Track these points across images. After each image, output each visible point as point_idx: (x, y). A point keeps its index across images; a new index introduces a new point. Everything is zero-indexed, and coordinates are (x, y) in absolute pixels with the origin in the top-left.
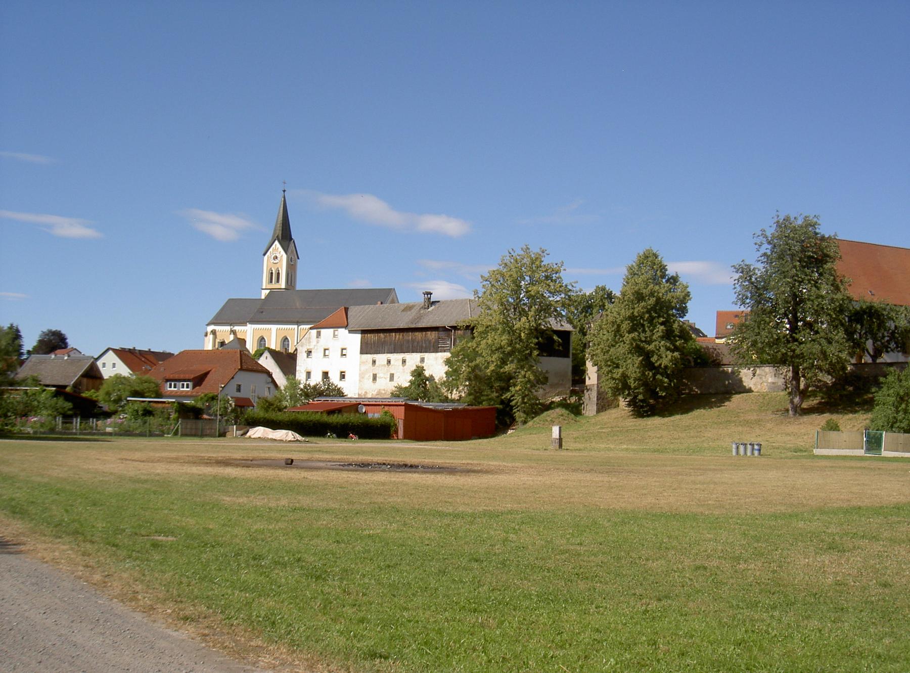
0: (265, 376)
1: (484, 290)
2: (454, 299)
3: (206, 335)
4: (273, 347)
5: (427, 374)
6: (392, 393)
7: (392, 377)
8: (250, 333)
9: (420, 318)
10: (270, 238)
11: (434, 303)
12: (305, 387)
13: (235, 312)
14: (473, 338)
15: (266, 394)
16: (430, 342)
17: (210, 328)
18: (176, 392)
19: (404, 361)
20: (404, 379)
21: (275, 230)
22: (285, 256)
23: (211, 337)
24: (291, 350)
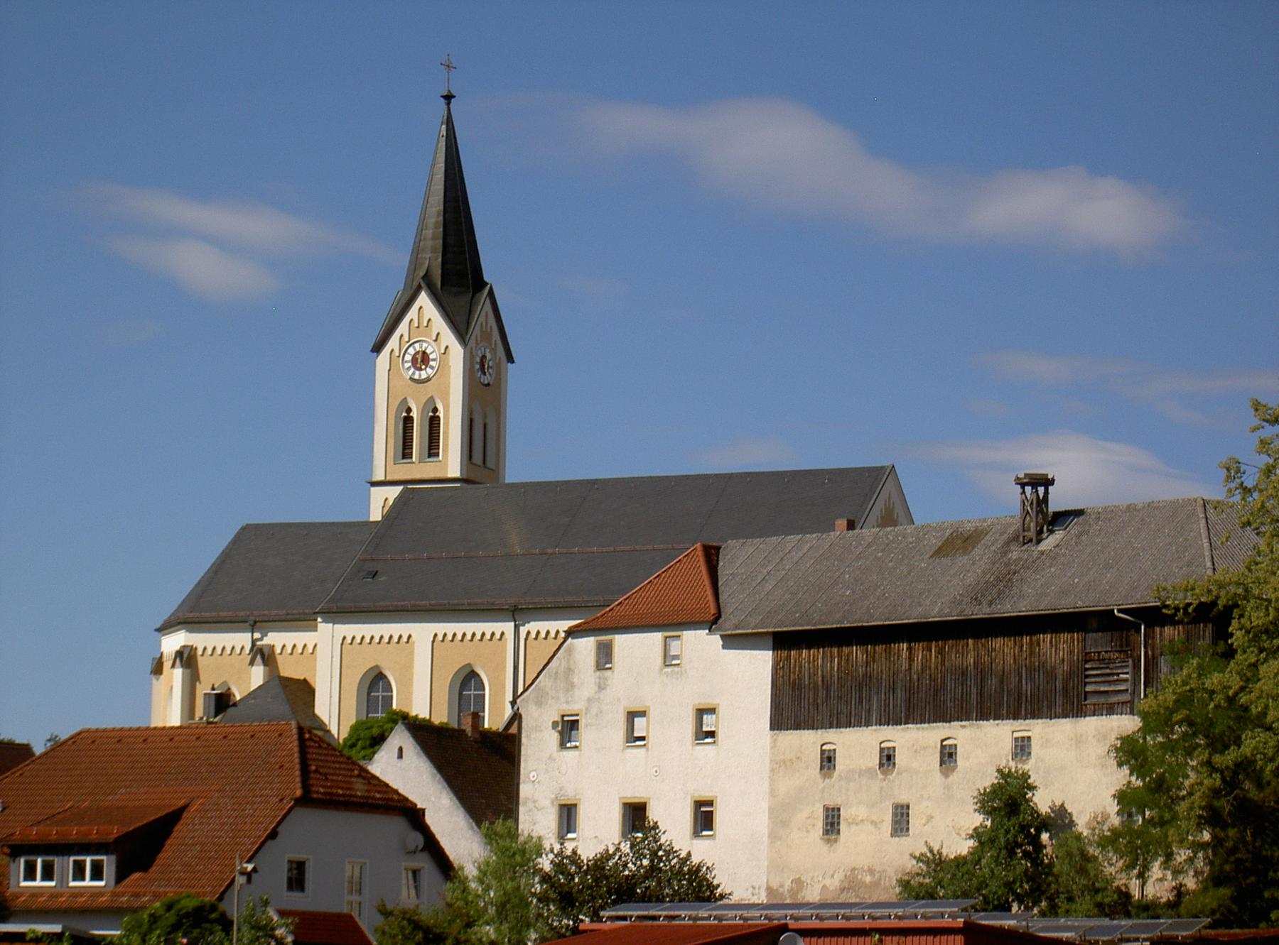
0: (398, 825)
1: (1264, 460)
2: (1123, 502)
3: (158, 669)
4: (420, 709)
5: (1043, 801)
6: (905, 884)
7: (901, 819)
8: (327, 659)
9: (1006, 579)
10: (396, 285)
11: (1061, 518)
12: (559, 867)
13: (266, 577)
14: (1230, 654)
15: (406, 897)
16: (1051, 675)
17: (172, 643)
18: (53, 894)
19: (948, 755)
20: (953, 826)
21: (417, 252)
22: (457, 352)
23: (176, 676)
24: (493, 720)
